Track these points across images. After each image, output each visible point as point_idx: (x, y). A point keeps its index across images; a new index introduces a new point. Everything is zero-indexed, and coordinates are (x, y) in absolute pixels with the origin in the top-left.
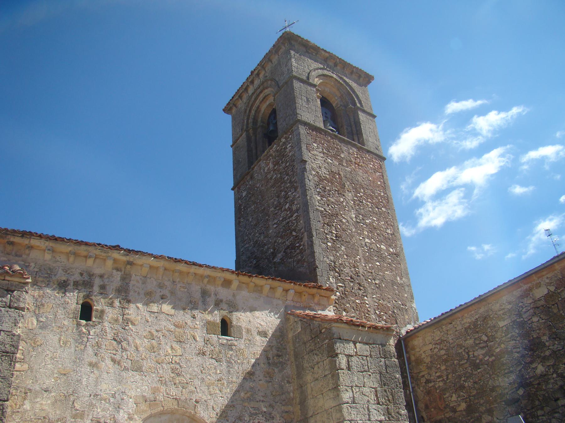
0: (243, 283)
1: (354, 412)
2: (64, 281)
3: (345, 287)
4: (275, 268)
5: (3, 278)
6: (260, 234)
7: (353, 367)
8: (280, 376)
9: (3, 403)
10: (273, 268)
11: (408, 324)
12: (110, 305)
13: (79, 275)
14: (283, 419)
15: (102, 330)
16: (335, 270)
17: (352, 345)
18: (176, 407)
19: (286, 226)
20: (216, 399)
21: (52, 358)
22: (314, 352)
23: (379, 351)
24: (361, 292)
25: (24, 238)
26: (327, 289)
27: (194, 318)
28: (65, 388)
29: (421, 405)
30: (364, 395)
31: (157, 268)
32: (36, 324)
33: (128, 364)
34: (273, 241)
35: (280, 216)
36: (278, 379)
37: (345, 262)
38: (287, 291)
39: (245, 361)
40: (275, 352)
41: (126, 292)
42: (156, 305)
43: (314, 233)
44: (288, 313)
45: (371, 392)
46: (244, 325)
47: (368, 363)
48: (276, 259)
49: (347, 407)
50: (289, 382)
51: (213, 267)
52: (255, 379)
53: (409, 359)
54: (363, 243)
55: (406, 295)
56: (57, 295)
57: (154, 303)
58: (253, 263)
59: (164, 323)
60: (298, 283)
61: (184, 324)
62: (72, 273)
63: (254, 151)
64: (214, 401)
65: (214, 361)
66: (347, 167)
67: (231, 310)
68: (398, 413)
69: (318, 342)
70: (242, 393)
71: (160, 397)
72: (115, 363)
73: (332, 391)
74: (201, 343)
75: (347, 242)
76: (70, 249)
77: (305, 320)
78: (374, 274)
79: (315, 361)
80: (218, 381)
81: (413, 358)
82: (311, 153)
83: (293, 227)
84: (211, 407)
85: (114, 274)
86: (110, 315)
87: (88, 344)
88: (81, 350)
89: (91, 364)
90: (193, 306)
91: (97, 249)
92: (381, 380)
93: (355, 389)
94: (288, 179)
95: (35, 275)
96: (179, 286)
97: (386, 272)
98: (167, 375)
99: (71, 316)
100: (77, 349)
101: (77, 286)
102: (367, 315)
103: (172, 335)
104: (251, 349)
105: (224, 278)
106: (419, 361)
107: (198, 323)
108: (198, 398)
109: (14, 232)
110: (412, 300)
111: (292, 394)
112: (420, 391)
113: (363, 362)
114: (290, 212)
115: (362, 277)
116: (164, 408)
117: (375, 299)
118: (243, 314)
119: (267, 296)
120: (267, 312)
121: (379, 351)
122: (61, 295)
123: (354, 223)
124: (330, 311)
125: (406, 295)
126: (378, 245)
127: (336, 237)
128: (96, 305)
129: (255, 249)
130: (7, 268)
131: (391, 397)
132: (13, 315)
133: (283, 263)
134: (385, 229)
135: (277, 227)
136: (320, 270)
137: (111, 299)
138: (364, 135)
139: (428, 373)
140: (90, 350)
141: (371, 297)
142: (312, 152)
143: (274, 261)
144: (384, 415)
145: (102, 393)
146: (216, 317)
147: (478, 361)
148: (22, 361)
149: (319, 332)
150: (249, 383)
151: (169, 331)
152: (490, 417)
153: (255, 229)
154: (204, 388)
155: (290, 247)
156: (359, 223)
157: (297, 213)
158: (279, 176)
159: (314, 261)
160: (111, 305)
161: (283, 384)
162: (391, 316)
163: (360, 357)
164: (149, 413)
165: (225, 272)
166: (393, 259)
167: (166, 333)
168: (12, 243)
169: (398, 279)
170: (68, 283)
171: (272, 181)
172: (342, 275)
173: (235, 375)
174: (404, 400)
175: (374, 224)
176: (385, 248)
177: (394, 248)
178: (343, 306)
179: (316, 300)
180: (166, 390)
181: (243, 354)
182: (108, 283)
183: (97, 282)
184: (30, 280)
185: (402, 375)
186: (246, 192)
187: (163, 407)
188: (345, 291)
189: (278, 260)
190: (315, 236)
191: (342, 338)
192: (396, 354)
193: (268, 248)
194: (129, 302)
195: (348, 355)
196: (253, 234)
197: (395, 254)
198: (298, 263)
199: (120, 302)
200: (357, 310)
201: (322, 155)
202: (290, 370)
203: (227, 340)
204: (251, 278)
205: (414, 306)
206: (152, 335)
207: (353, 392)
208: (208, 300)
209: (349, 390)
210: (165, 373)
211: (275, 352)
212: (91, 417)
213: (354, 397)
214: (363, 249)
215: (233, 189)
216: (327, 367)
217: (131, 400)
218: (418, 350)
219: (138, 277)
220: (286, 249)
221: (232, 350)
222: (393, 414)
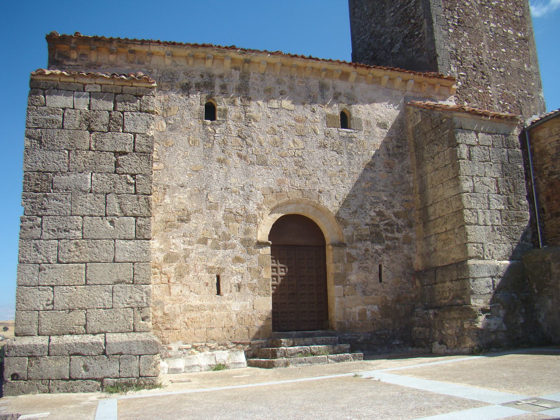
0: (361, 75)
1: (473, 201)
2: (187, 84)
3: (467, 76)
4: (393, 58)
5: (131, 85)
6: (376, 24)
7: (475, 157)
8: (400, 166)
9: (148, 196)
10: (391, 60)
11: (534, 114)
12: (232, 103)
13: (200, 77)
14: (403, 208)
15: (227, 129)
16: (457, 58)
17: (473, 134)
18: (301, 197)
19: (403, 13)
20: (338, 189)
21: (184, 157)
22: (434, 142)
23: (502, 140)
24: (484, 81)
25: (144, 45)
26: (448, 79)
27: (314, 112)
28: (198, 183)
29: (543, 198)
30: (485, 184)
31: (274, 65)
32: (165, 126)
33: (254, 159)
34: (391, 31)
36: (398, 170)
37: (468, 50)
38: (406, 81)
39: (365, 153)
40: (395, 143)
42: (276, 101)
43: (434, 19)
44: (408, 104)
45: (492, 182)
46: (363, 117)
47: (489, 153)
48: (394, 50)
49: (467, 196)
50: (409, 172)
51: (330, 60)
52: (375, 170)
53: (532, 150)
54: (488, 28)
55: (533, 84)
56: (181, 97)
57: (274, 99)
59: (285, 119)
60: (418, 73)
61: (305, 119)
62: (192, 76)
64: (337, 191)
65: (335, 153)
67: (350, 103)
68: (518, 203)
69: (439, 132)
70: (363, 183)
71: (286, 189)
72: (241, 158)
73: (453, 180)
75: (470, 28)
76: (188, 52)
77: (425, 110)
78: (499, 61)
79: (435, 151)
80: (339, 172)
81: (537, 150)
83: (411, 14)
84: (334, 197)
85: (232, 73)
86: (233, 114)
87: (215, 142)
88: (209, 148)
89: (219, 161)
90: (312, 100)
91: (214, 50)
92: (502, 170)
93: (476, 179)
95: (159, 81)
96: (297, 81)
97: (513, 60)
98: (291, 168)
99: (197, 117)
100: (205, 147)
101: (199, 88)
102: (490, 105)
103: (293, 130)
104: (370, 141)
105: (342, 71)
106: (543, 153)
107: (318, 117)
108: (321, 189)
109: (134, 41)
110: (539, 89)
111: (411, 184)
112: (542, 184)
113: (485, 152)
115: (485, 65)
116: (289, 199)
117: (499, 89)
118: (362, 106)
119: (386, 88)
120: (386, 103)
121: (502, 140)
122: (185, 97)
123: (478, 6)
124: (451, 101)
125: (533, 84)
126: (504, 30)
127: (458, 22)
128: (219, 105)
129: (371, 40)
130: (132, 75)
131: (512, 187)
132: (144, 118)
134: (513, 12)
135: (393, 15)
136: (440, 58)
137: (232, 98)
139: (552, 165)
140: (217, 148)
141: (494, 86)
143: (392, 51)
144: (504, 204)
145: (232, 187)
146: (336, 110)
148: (158, 161)
149: (439, 122)
150: (370, 174)
151: (290, 126)
153: (371, 20)
154: (327, 179)
155: (409, 35)
156: (484, 5)
159: (435, 49)
160: (233, 103)
161: (403, 174)
162: (516, 106)
163: (482, 147)
164: (276, 203)
165: (342, 64)
166: (520, 45)
167: (288, 127)
168: (133, 52)
169: (526, 66)
170: (190, 85)
172: (464, 64)
173: (355, 166)
174: (526, 190)
175: (501, 6)
176: (512, 33)
177: (523, 32)
178: (464, 96)
179: (437, 90)
180: (291, 182)
181: (363, 145)
182: (228, 83)
183: (218, 82)
184: (155, 85)
185: (525, 165)
187: (288, 197)
188: (467, 80)
189: (396, 51)
190: (435, 22)
191: (463, 128)
192: (519, 144)
193: (386, 39)
194: (249, 99)
195: (469, 145)
197: (524, 39)
198: (417, 52)
199: (241, 100)
200: (479, 100)
202: (409, 161)
203: (347, 132)
204: (369, 69)
205: (542, 96)
206: (274, 130)
207: (473, 181)
208: (327, 93)
209: (469, 180)
210: (288, 166)
211: (395, 143)
212: (224, 208)
213: (474, 187)
214: (487, 34)
216: (448, 157)
217: (258, 192)
218: (542, 141)
219: (256, 75)
220: (404, 38)
221: (352, 142)
222: (513, 204)
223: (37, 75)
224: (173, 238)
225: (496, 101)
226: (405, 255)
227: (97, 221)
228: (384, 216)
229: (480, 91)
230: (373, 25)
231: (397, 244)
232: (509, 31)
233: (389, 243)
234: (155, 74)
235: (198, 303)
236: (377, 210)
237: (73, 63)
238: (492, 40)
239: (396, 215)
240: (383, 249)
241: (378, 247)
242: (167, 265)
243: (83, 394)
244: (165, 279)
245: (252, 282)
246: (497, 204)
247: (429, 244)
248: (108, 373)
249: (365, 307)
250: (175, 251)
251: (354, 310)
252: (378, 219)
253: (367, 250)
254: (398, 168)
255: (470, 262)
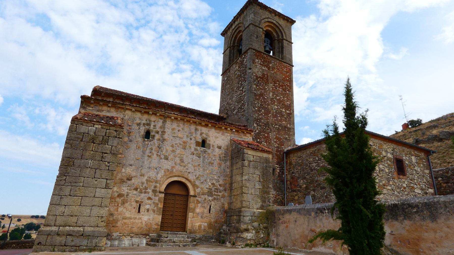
2: (139, 123)
6: (230, 99)
40: (224, 155)
41: (164, 128)
55: (291, 133)
63: (232, 58)
66: (272, 71)
74: (193, 150)
81: (288, 162)
97: (283, 122)
125: (291, 133)
147: (313, 168)
152: (314, 193)
154: (192, 168)
166: (287, 116)
171: (237, 75)
193: (232, 106)
201: (260, 65)
211: (224, 155)
212: (147, 176)
215: (221, 75)
221: (205, 153)
223: (75, 119)
224: (123, 187)
226: (222, 202)
227: (90, 180)
228: (214, 185)
231: (219, 198)
232: (283, 110)
233: (215, 197)
234: (127, 117)
235: (129, 216)
236: (212, 182)
237: (91, 109)
239: (220, 185)
240: (212, 199)
241: (210, 198)
242: (118, 198)
243: (69, 253)
244: (116, 204)
245: (154, 208)
246: (258, 186)
247: (231, 199)
248: (82, 244)
249: (201, 224)
250: (123, 193)
251: (196, 224)
252: (212, 186)
253: (205, 199)
254: (223, 166)
255: (243, 209)
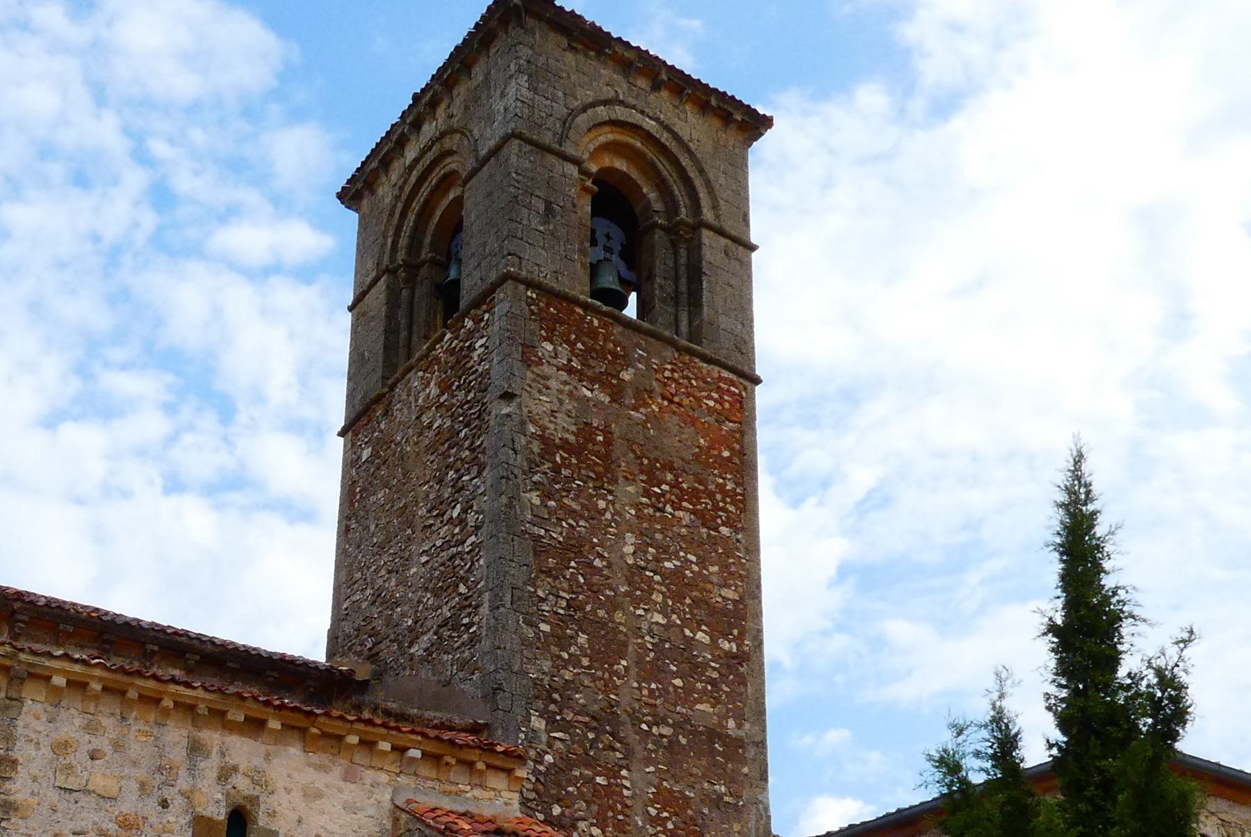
6: (389, 572)
16: (550, 696)
35: (439, 534)
48: (416, 648)
58: (366, 646)
63: (404, 334)
82: (533, 372)
90: (163, 778)
94: (466, 438)
102: (621, 817)
114: (462, 530)
133: (429, 662)
135: (427, 562)
138: (705, 309)
142: (535, 369)
143: (412, 651)
157: (476, 535)
158: (448, 423)
166: (724, 671)
171: (431, 434)
175: (687, 572)
177: (733, 640)
186: (370, 449)
196: (373, 568)
214: (639, 641)
219: (39, 705)
220: (440, 626)
225: (638, 807)
229: (599, 780)
230: (383, 572)
232: (700, 635)
238: (652, 654)
